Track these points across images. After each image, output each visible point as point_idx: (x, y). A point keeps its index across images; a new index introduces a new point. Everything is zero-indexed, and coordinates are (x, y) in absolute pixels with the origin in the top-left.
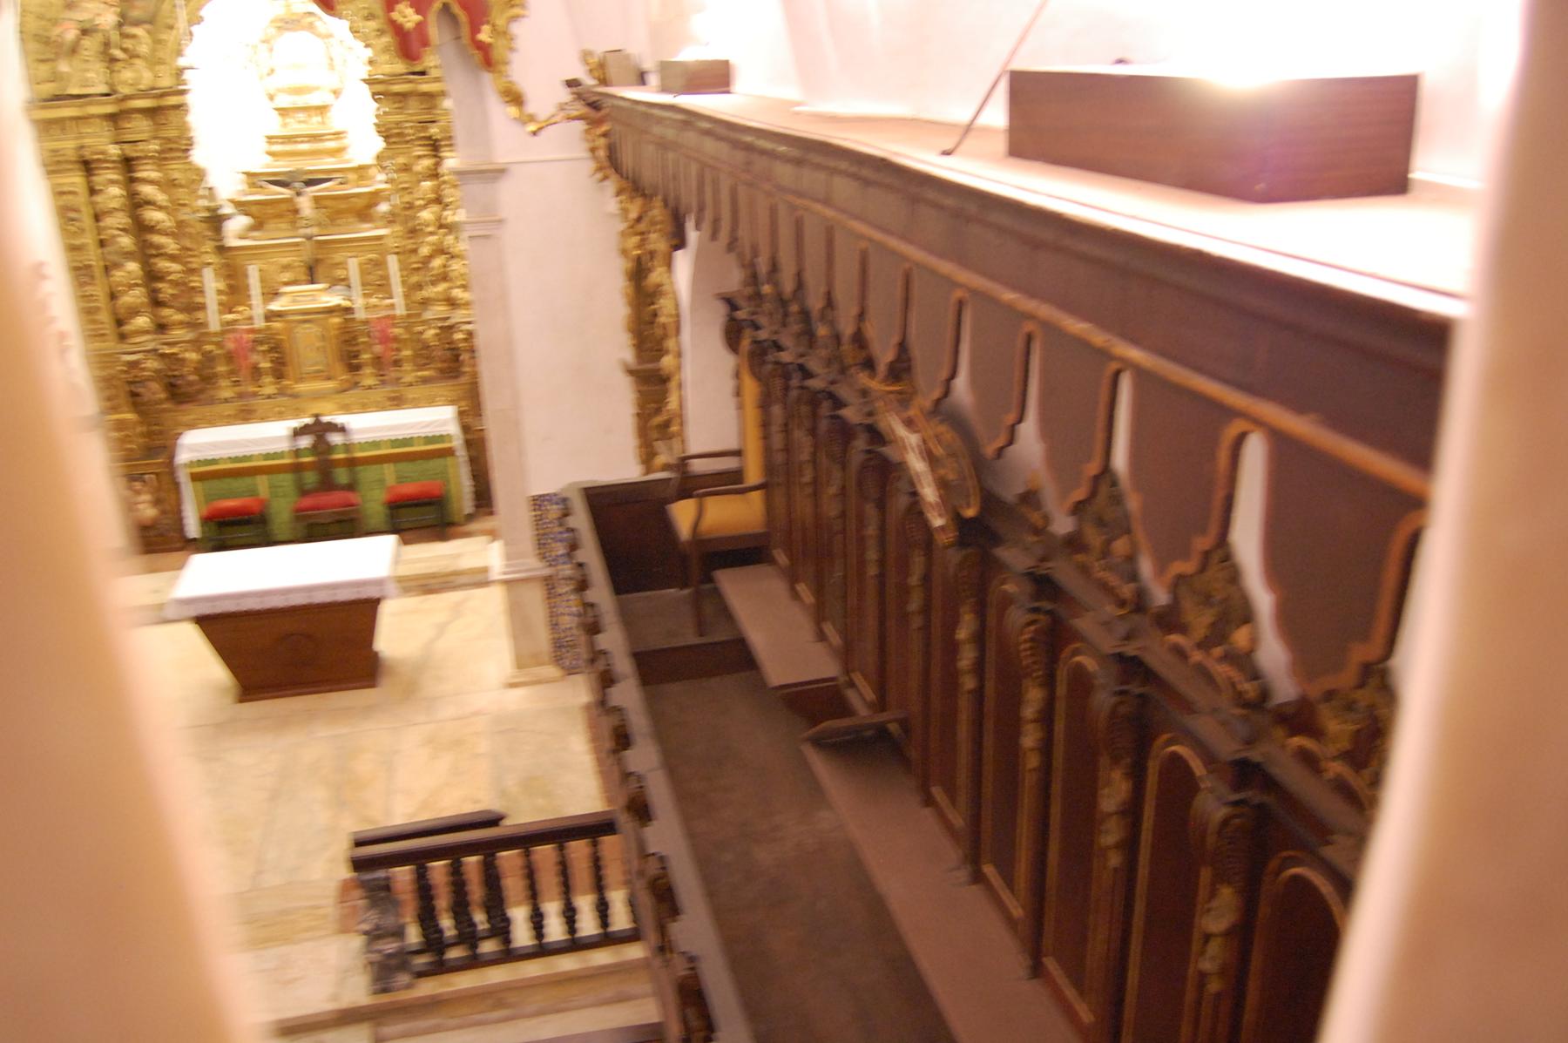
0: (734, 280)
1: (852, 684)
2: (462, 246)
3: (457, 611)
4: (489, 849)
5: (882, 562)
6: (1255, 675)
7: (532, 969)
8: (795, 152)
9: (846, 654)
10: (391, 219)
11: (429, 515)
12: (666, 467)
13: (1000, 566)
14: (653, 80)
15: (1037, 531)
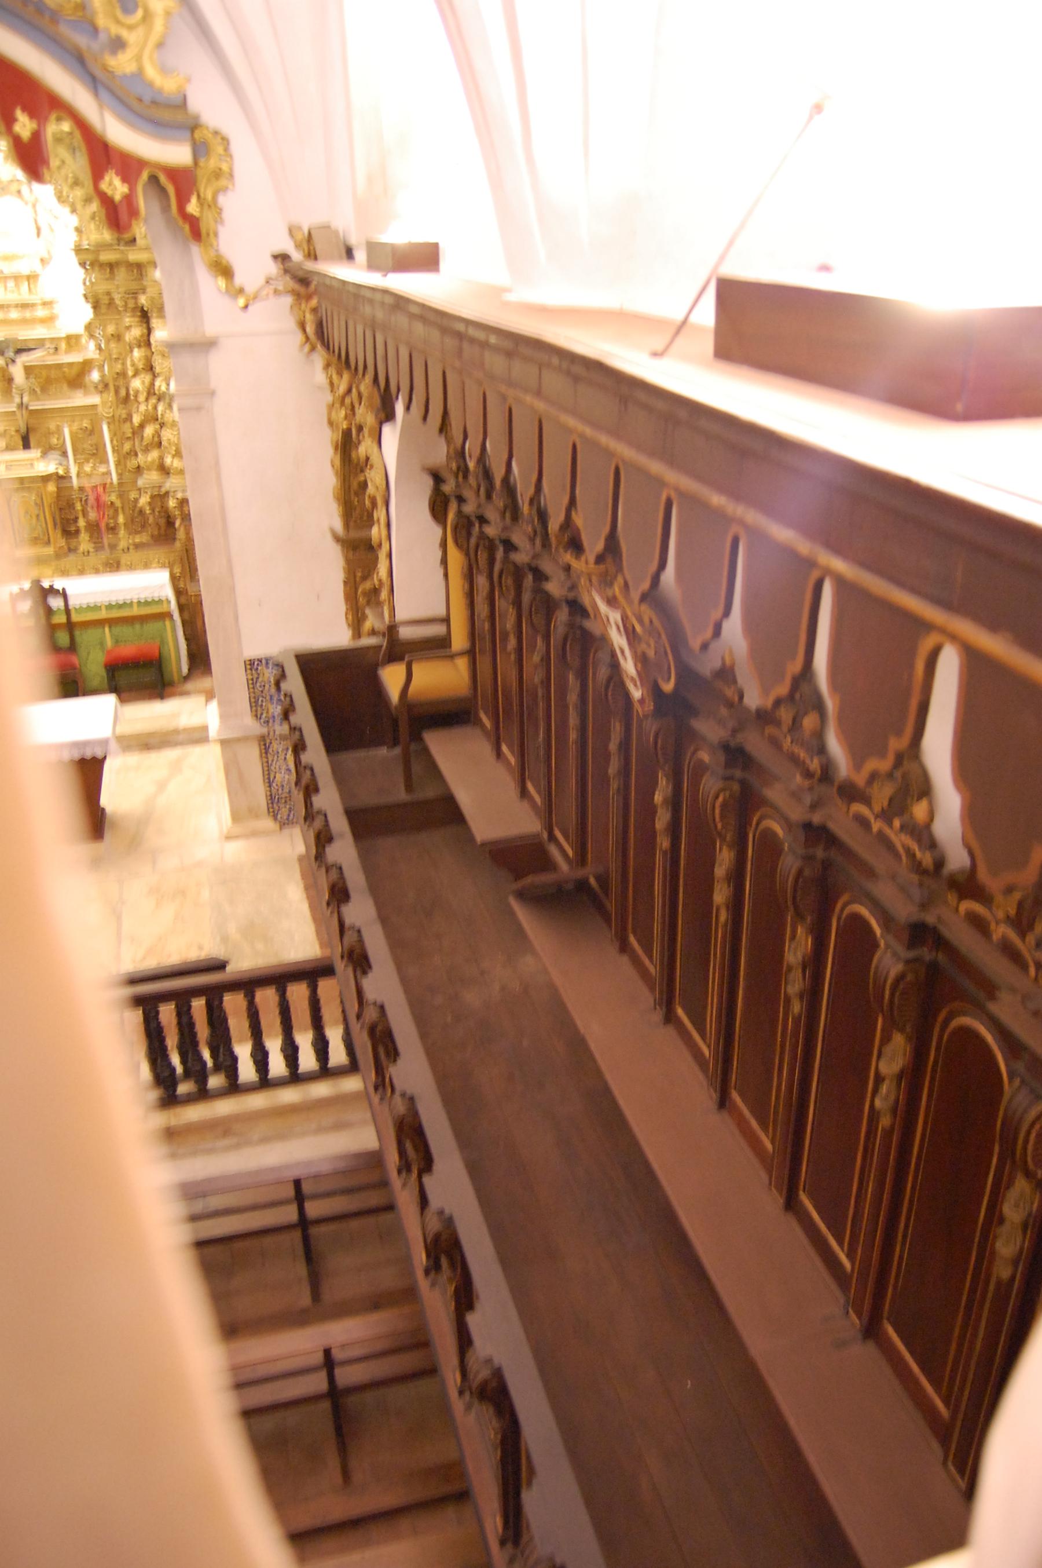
0: (439, 454)
1: (552, 837)
2: (175, 415)
3: (176, 767)
4: (214, 994)
5: (583, 729)
6: (933, 845)
7: (257, 1101)
8: (508, 344)
9: (548, 814)
10: (103, 387)
11: (148, 676)
12: (373, 632)
13: (693, 735)
14: (360, 256)
15: (730, 705)
